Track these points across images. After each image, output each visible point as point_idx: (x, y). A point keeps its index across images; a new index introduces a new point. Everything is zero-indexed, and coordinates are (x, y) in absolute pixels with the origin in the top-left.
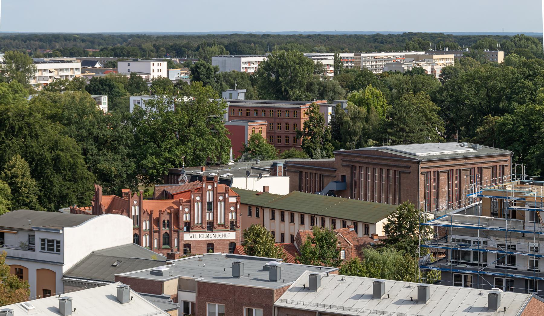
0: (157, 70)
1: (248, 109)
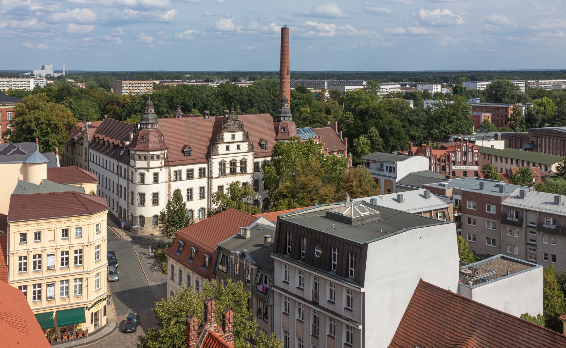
0: (436, 88)
1: (482, 107)
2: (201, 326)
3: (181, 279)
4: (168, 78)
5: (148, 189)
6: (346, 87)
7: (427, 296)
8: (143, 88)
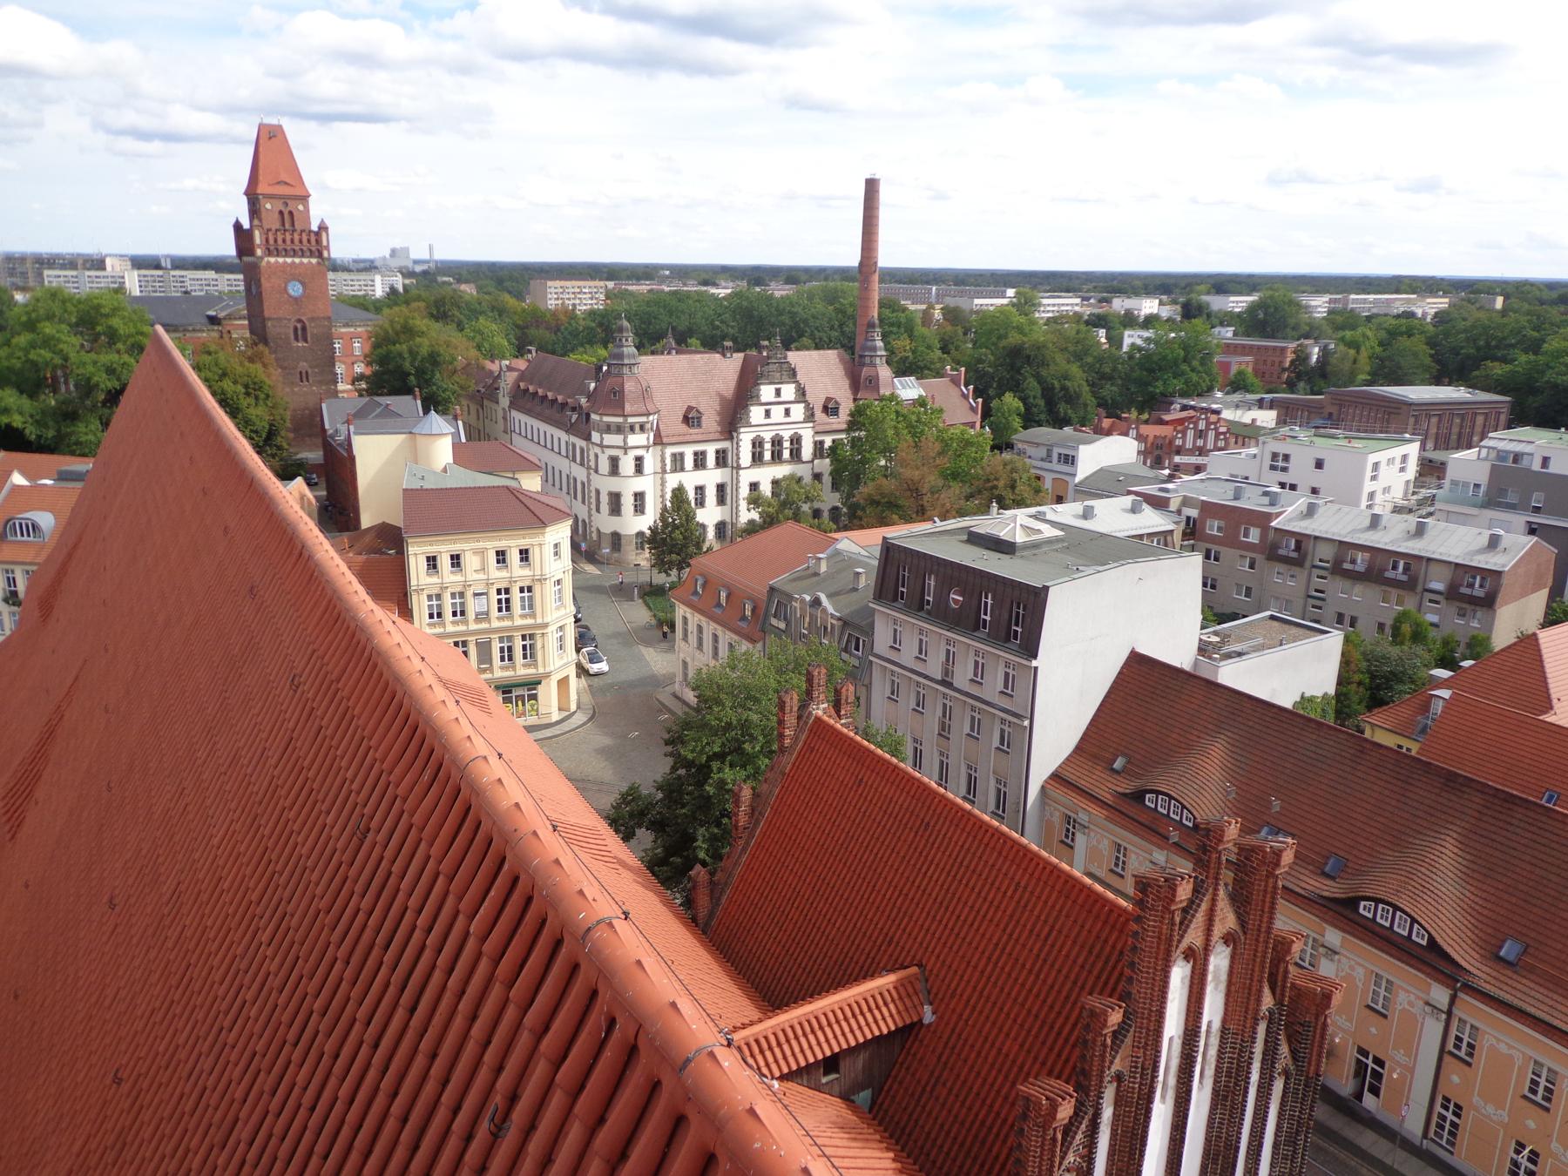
0: (1149, 306)
1: (1236, 346)
2: (804, 706)
3: (700, 640)
4: (629, 278)
5: (629, 485)
6: (977, 301)
7: (1141, 676)
8: (586, 298)
